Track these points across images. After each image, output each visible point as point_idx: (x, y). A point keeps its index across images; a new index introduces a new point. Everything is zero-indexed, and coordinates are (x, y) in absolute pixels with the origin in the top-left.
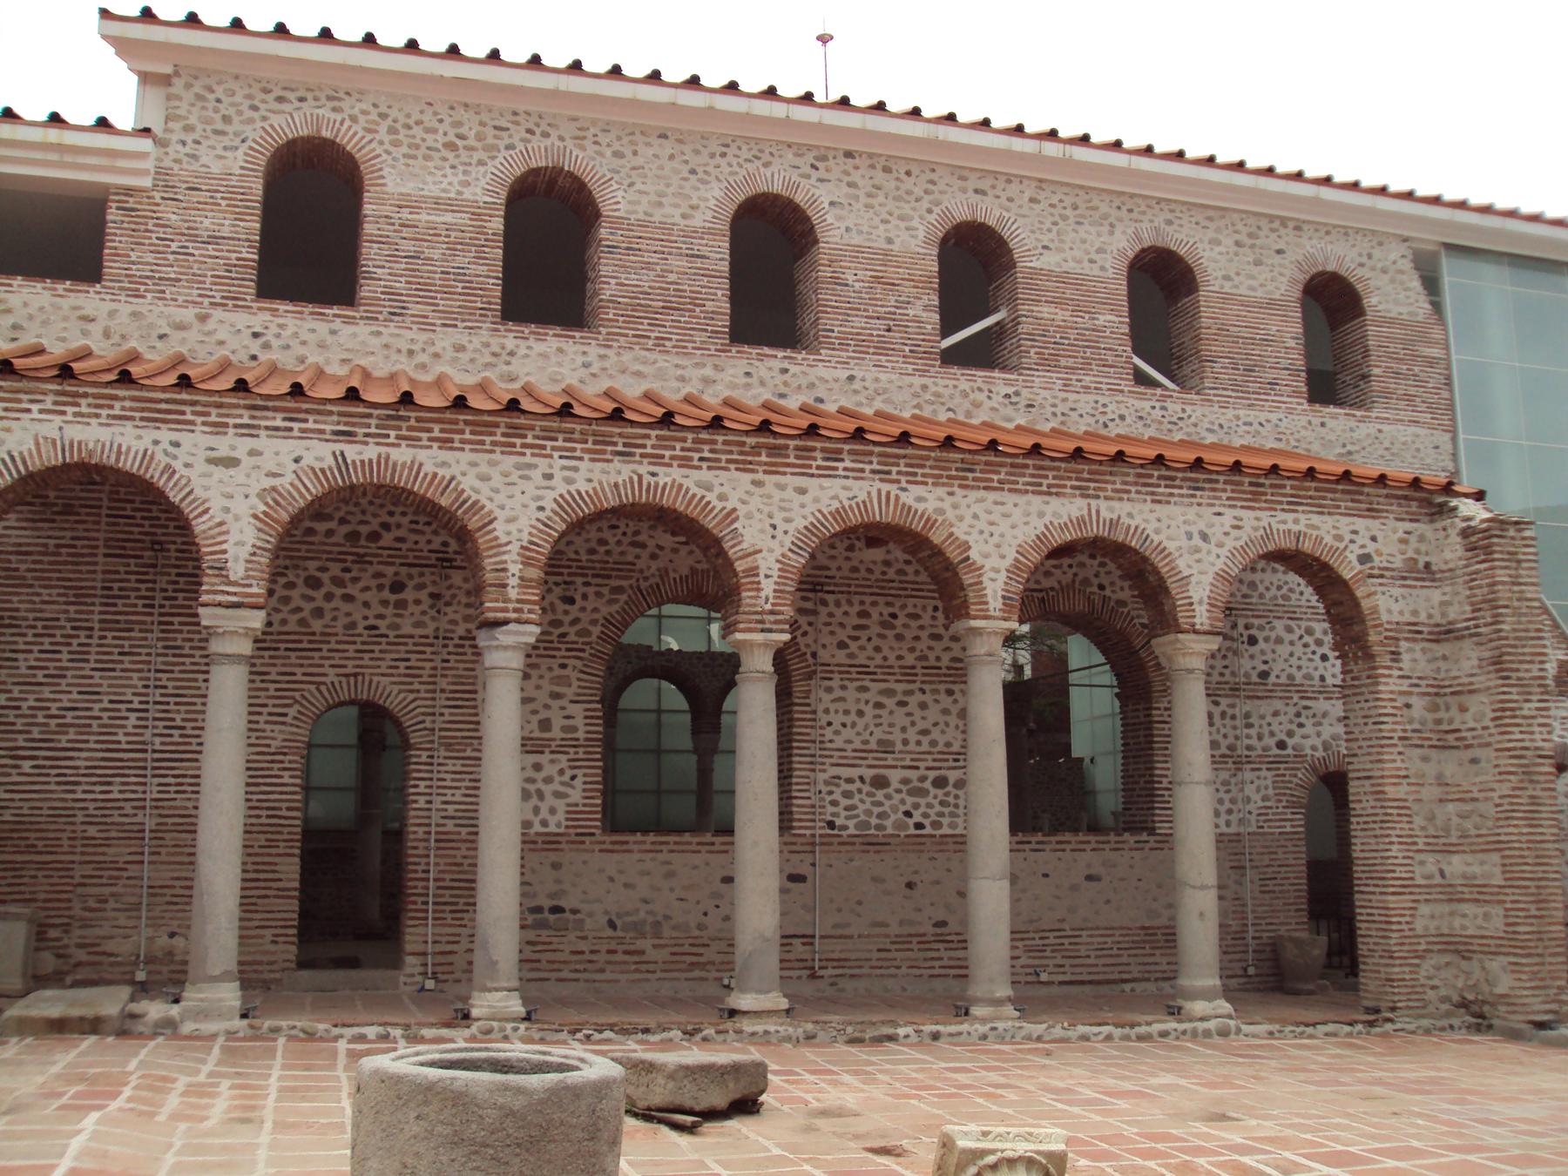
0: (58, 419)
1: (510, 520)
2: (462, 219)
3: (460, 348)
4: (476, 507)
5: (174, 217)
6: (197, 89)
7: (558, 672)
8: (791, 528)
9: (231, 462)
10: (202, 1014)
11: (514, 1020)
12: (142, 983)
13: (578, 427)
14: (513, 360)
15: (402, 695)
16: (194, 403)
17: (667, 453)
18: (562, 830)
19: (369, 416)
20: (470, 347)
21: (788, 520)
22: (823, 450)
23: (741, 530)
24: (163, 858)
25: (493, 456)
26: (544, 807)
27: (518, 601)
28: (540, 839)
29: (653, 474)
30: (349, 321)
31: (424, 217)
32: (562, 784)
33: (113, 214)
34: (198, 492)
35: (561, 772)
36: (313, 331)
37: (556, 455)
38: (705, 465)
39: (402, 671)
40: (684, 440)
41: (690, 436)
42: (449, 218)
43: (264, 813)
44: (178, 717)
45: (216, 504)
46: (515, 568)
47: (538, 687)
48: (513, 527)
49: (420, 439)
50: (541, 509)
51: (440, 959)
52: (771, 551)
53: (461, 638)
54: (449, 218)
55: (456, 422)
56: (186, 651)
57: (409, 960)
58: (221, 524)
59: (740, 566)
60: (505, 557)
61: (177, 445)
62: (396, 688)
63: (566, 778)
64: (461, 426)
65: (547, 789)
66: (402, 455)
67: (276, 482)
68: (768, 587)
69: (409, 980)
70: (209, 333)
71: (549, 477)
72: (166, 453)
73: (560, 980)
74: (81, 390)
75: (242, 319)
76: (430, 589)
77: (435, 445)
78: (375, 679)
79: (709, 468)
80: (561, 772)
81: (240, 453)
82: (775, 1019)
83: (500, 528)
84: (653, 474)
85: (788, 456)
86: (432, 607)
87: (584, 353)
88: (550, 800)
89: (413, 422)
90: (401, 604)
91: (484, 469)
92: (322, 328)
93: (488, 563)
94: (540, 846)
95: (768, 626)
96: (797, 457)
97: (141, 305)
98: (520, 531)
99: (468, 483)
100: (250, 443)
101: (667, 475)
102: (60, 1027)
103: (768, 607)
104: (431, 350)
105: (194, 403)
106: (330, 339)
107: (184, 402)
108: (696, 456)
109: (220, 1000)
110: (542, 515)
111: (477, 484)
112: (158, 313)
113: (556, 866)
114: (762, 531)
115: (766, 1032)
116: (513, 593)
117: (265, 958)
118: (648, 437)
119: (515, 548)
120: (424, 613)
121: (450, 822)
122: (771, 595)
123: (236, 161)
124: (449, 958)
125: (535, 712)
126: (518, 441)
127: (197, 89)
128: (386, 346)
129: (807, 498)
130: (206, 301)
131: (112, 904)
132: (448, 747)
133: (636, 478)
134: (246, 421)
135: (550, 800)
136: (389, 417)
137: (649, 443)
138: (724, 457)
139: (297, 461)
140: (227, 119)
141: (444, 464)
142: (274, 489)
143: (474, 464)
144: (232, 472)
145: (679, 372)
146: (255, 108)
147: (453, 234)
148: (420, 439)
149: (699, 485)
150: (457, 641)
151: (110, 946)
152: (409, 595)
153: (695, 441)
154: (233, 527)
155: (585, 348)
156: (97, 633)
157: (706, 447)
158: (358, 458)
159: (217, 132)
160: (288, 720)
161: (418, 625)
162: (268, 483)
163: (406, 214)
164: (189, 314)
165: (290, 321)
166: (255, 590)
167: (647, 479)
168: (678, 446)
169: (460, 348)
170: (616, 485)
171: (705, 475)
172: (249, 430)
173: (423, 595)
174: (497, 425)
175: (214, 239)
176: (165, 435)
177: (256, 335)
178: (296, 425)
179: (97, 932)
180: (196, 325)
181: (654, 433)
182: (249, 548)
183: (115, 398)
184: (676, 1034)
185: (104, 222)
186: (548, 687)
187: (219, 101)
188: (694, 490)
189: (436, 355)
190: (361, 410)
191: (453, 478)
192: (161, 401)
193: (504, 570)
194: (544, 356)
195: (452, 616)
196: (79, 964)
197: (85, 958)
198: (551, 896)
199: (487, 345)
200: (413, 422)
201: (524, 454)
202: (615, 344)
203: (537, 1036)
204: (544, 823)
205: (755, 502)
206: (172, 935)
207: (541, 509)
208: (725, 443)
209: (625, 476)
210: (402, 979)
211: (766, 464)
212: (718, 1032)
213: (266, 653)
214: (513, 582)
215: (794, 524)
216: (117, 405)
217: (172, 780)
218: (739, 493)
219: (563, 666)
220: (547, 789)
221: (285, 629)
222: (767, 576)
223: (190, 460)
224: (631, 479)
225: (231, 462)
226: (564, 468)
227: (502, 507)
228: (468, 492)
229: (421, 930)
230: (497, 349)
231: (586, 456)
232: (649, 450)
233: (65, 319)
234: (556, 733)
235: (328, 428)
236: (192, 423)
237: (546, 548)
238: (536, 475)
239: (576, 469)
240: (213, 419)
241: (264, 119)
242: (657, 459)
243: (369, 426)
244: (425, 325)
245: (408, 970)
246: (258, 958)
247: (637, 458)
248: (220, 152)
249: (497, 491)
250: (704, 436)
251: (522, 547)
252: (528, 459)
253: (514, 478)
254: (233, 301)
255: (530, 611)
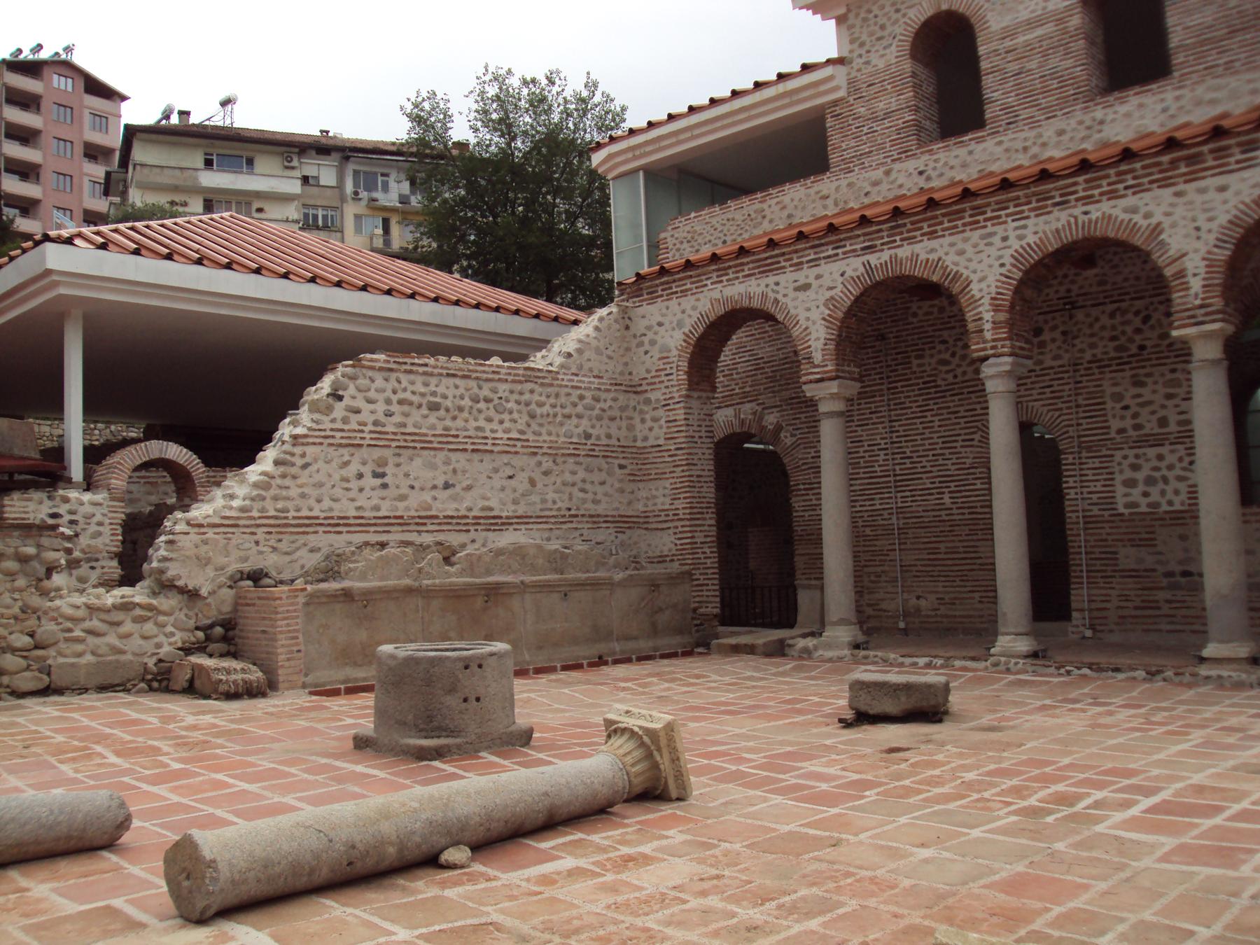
0: (719, 286)
1: (981, 280)
2: (1049, 28)
3: (1061, 133)
4: (957, 275)
5: (862, 110)
6: (863, 15)
7: (1169, 376)
8: (1214, 225)
9: (806, 287)
10: (829, 646)
11: (1019, 657)
12: (904, 629)
13: (1020, 193)
14: (1105, 127)
15: (1050, 414)
16: (783, 254)
17: (1096, 192)
18: (1186, 508)
19: (880, 231)
20: (1069, 129)
21: (1210, 219)
22: (1239, 144)
23: (1168, 240)
24: (908, 546)
25: (965, 235)
26: (1169, 489)
27: (994, 340)
28: (1167, 516)
29: (1086, 213)
30: (980, 140)
31: (1021, 39)
32: (1184, 469)
33: (829, 122)
34: (793, 312)
35: (1181, 459)
36: (956, 157)
37: (1009, 219)
38: (1130, 192)
39: (1049, 395)
40: (1107, 176)
41: (1112, 171)
42: (1039, 32)
43: (966, 511)
44: (908, 450)
45: (802, 316)
46: (988, 316)
47: (1154, 392)
48: (983, 285)
49: (915, 237)
50: (1002, 265)
51: (1095, 614)
52: (1196, 251)
53: (1089, 362)
54: (1039, 32)
55: (936, 217)
56: (908, 405)
57: (1074, 614)
58: (806, 328)
59: (1168, 272)
60: (980, 309)
61: (777, 284)
62: (1046, 408)
63: (1185, 464)
64: (941, 219)
65: (1171, 475)
66: (904, 252)
67: (832, 293)
68: (1196, 284)
69: (1074, 629)
70: (892, 183)
71: (1005, 239)
72: (773, 291)
73: (1194, 632)
74: (726, 265)
75: (911, 165)
76: (1061, 329)
77: (925, 238)
78: (1031, 404)
79: (1134, 194)
80: (1181, 459)
81: (811, 280)
82: (1235, 666)
83: (975, 288)
84: (1086, 213)
85: (1204, 161)
86: (1064, 342)
87: (1162, 100)
88: (1174, 484)
89: (909, 226)
90: (1042, 345)
91: (960, 246)
92: (962, 152)
93: (969, 316)
94: (1169, 522)
95: (1201, 319)
96: (1215, 159)
97: (852, 177)
98: (989, 286)
99: (949, 260)
100: (816, 271)
101: (1098, 210)
102: (736, 649)
103: (1198, 302)
104: (1040, 141)
105: (783, 254)
106: (969, 159)
107: (777, 256)
108: (1121, 186)
109: (837, 637)
110: (1003, 270)
111: (957, 258)
112: (862, 178)
113: (1183, 538)
114: (1186, 236)
115: (1220, 677)
116: (988, 335)
117: (976, 613)
118: (1075, 184)
119: (986, 301)
120: (1059, 348)
121: (1095, 508)
122: (1200, 290)
123: (892, 54)
124: (1104, 614)
125: (1153, 413)
126: (981, 218)
127: (863, 15)
128: (1007, 150)
129: (1227, 194)
130: (889, 160)
131: (883, 578)
132: (1089, 449)
133: (1072, 220)
134: (812, 257)
135: (1174, 484)
136: (892, 228)
137: (1080, 188)
138: (1145, 180)
139: (842, 275)
140: (883, 27)
141: (932, 250)
142: (832, 298)
143: (952, 245)
144: (808, 293)
145: (1251, 86)
146: (897, 11)
147: (1044, 43)
148: (915, 237)
149: (1126, 211)
150: (1086, 365)
151: (884, 606)
152: (1046, 336)
153: (1119, 174)
154: (812, 329)
155: (1162, 96)
156: (856, 402)
157: (1129, 176)
158: (877, 263)
159: (879, 39)
160: (975, 443)
161: (1055, 358)
162: (828, 294)
163: (1008, 43)
164: (879, 174)
165: (942, 156)
166: (830, 368)
167: (1081, 218)
168: (1104, 182)
169: (1061, 133)
170: (1057, 231)
171: (1130, 201)
172: (814, 263)
173: (1057, 334)
174: (964, 210)
175: (887, 115)
176: (771, 279)
177: (921, 173)
178: (840, 251)
179: (877, 596)
180: (885, 180)
181: (1080, 179)
182: (822, 341)
183: (742, 264)
184: (1141, 674)
185: (824, 129)
186: (1163, 390)
187: (876, 16)
188: (1123, 216)
189: (1044, 145)
190: (875, 228)
191: (940, 259)
192: (766, 258)
193: (980, 319)
194: (1128, 115)
195: (1079, 346)
196: (869, 617)
197: (872, 613)
198: (1180, 563)
199: (1081, 123)
200: (909, 226)
201: (985, 227)
202: (1188, 82)
203: (1030, 669)
204: (1170, 503)
205: (1179, 211)
206: (918, 598)
207: (1002, 265)
208: (1144, 167)
209: (1063, 221)
210: (1070, 629)
211: (1185, 174)
212: (1176, 674)
213: (956, 398)
214: (988, 326)
215: (1217, 222)
216: (746, 268)
217: (908, 494)
218: (1164, 208)
219: (1173, 371)
220: (1171, 475)
221: (966, 378)
222: (1195, 275)
223: (785, 292)
224: (1069, 224)
225: (806, 287)
226: (1016, 228)
227: (974, 272)
228: (951, 266)
229: (1080, 591)
230: (1088, 123)
231: (1032, 214)
232: (1081, 194)
233: (814, 201)
234: (1173, 427)
235: (858, 247)
236: (784, 267)
237: (1008, 295)
238: (996, 240)
239: (1025, 227)
240: (795, 261)
241: (904, 15)
242: (1088, 200)
243: (882, 238)
244: (1033, 123)
245: (1074, 622)
246: (971, 613)
247: (1073, 203)
248: (882, 52)
249: (970, 260)
250: (1123, 167)
251: (992, 299)
252: (990, 229)
253: (981, 247)
254: (906, 154)
255: (1003, 347)
